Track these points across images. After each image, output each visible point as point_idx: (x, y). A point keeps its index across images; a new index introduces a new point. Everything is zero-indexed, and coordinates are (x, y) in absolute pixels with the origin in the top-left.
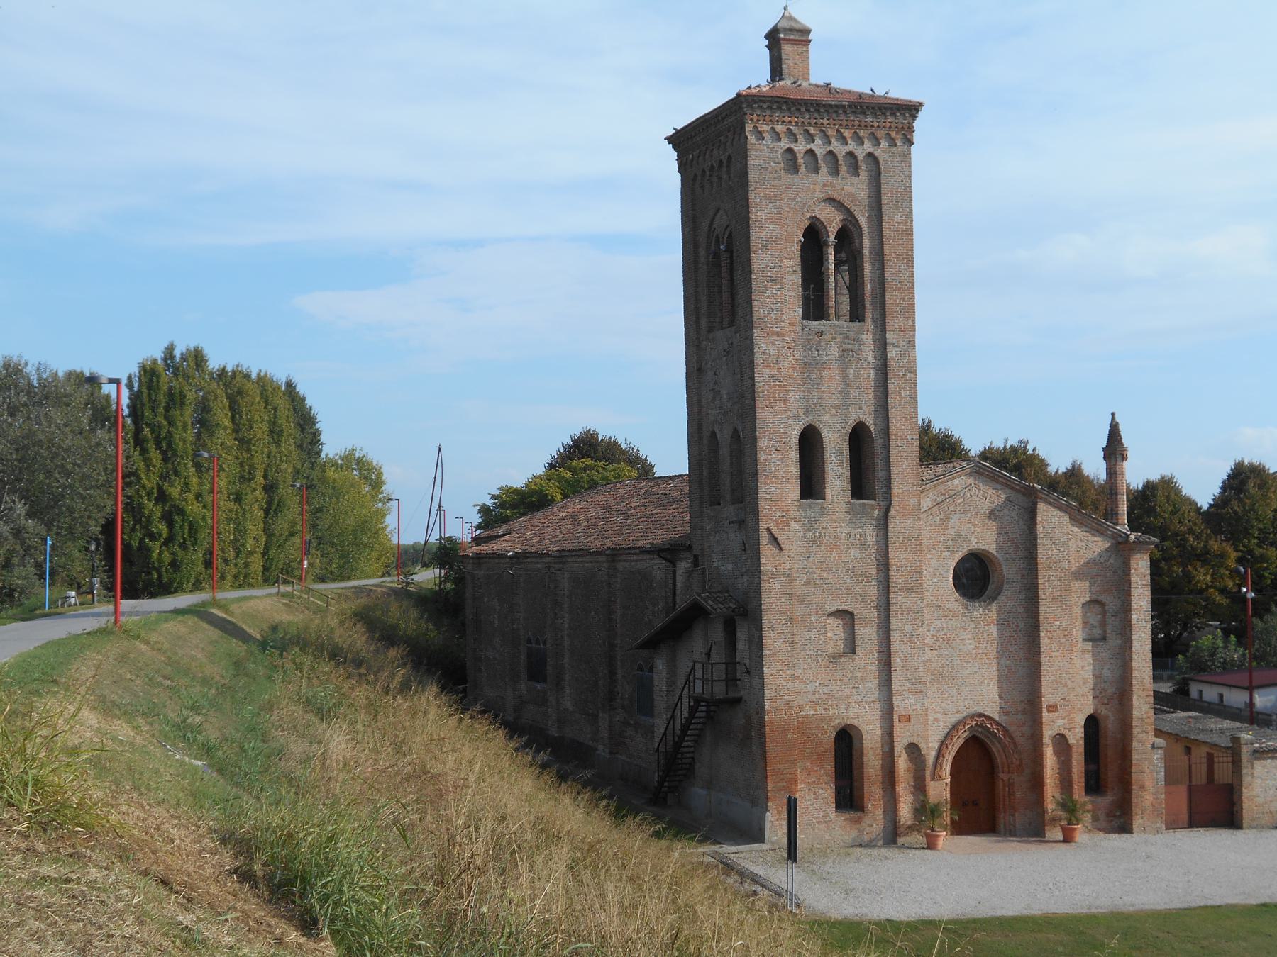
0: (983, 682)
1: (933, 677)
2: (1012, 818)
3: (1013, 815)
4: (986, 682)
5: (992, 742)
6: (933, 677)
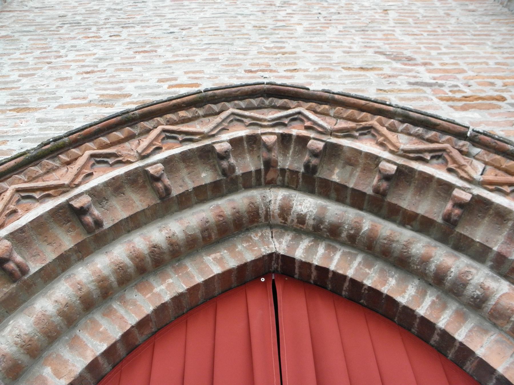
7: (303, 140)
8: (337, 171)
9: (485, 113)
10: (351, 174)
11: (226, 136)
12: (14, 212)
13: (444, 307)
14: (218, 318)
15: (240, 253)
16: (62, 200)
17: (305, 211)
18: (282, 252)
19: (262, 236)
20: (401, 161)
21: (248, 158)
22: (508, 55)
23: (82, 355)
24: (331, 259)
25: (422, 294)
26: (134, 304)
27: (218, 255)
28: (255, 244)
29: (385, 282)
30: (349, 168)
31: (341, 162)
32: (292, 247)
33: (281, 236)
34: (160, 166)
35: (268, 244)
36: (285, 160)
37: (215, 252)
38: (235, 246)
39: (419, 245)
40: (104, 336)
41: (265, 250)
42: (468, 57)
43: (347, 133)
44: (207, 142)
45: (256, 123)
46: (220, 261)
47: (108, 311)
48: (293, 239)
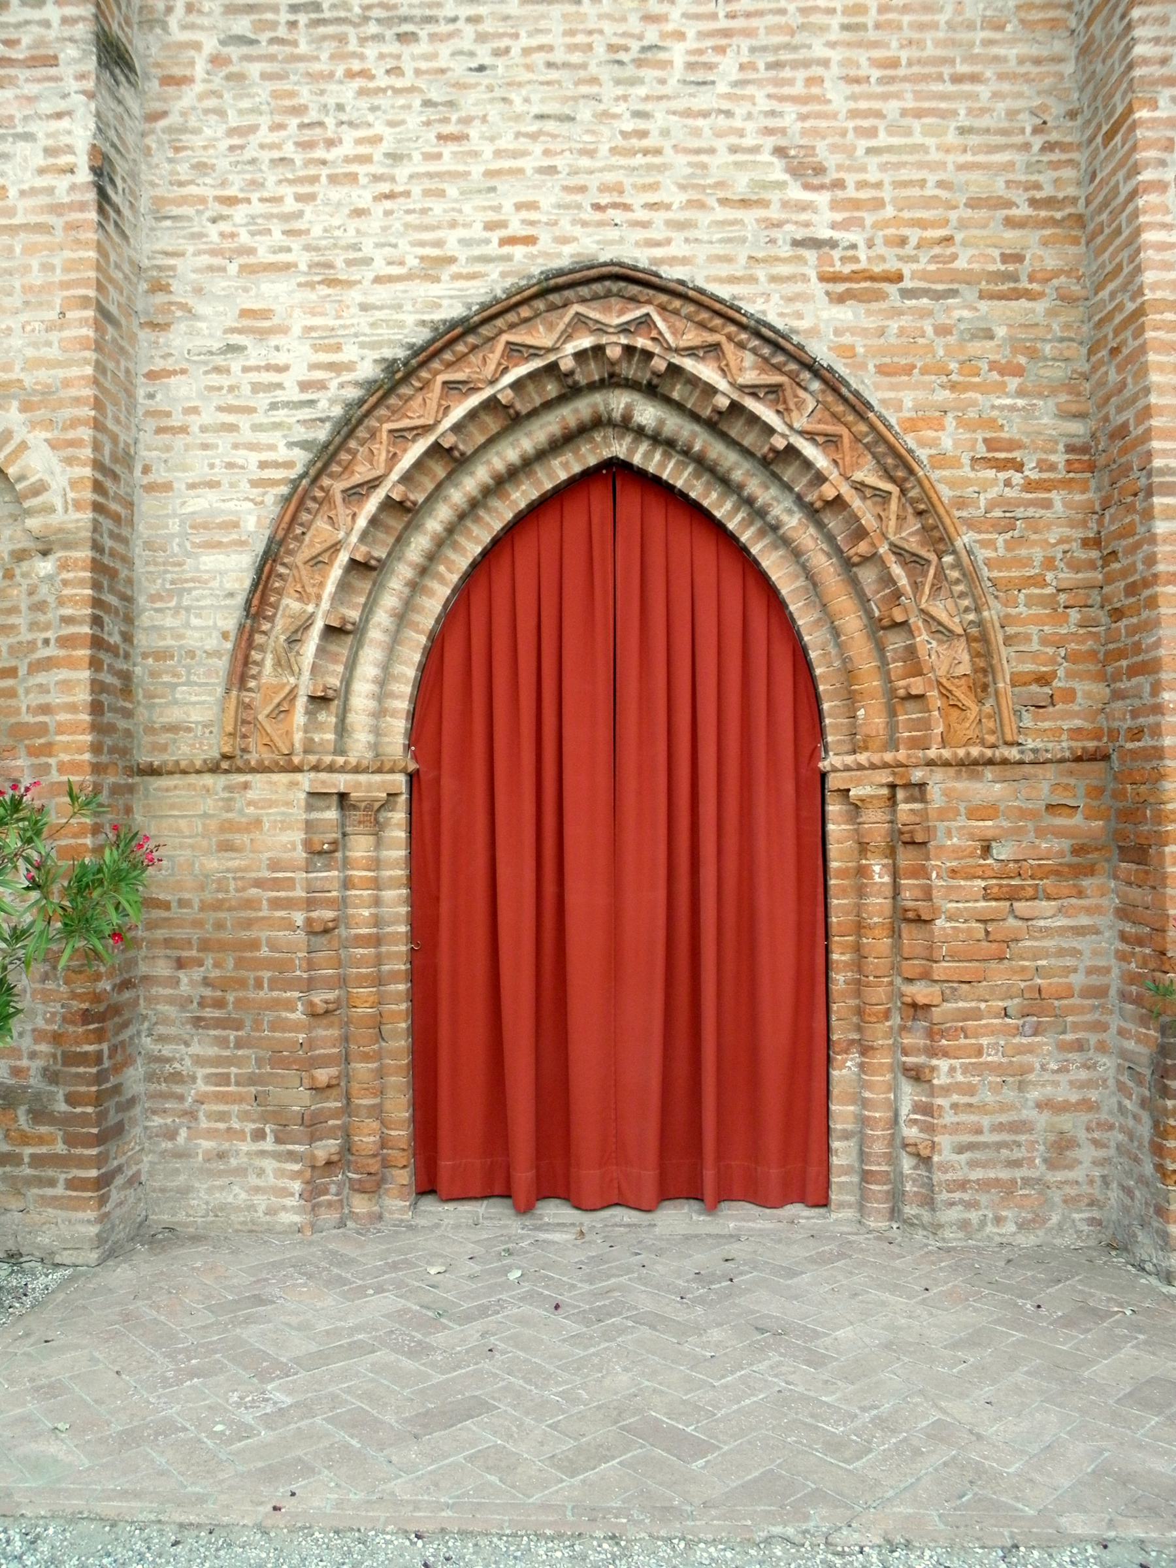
0: (650, 55)
1: (242, 25)
2: (909, 1095)
3: (917, 1075)
4: (678, 53)
5: (758, 513)
6: (242, 25)
7: (648, 355)
8: (678, 387)
9: (862, 308)
10: (691, 393)
11: (570, 348)
12: (395, 454)
13: (751, 523)
14: (566, 524)
15: (584, 456)
16: (430, 439)
17: (644, 422)
18: (622, 457)
19: (604, 437)
20: (735, 396)
21: (593, 365)
22: (968, 158)
23: (464, 555)
24: (665, 467)
25: (736, 509)
26: (496, 510)
27: (563, 459)
28: (597, 446)
29: (707, 496)
30: (689, 387)
31: (683, 380)
32: (632, 451)
33: (622, 437)
34: (509, 391)
35: (609, 446)
36: (629, 367)
37: (561, 455)
38: (579, 449)
39: (739, 472)
40: (477, 541)
41: (606, 454)
42: (903, 164)
43: (691, 351)
44: (552, 358)
45: (601, 329)
46: (566, 465)
47: (417, 384)
48: (634, 441)
